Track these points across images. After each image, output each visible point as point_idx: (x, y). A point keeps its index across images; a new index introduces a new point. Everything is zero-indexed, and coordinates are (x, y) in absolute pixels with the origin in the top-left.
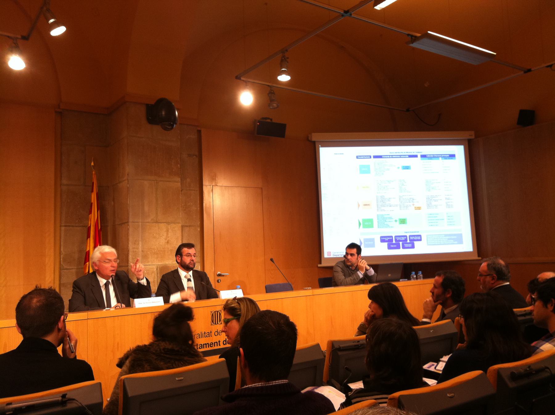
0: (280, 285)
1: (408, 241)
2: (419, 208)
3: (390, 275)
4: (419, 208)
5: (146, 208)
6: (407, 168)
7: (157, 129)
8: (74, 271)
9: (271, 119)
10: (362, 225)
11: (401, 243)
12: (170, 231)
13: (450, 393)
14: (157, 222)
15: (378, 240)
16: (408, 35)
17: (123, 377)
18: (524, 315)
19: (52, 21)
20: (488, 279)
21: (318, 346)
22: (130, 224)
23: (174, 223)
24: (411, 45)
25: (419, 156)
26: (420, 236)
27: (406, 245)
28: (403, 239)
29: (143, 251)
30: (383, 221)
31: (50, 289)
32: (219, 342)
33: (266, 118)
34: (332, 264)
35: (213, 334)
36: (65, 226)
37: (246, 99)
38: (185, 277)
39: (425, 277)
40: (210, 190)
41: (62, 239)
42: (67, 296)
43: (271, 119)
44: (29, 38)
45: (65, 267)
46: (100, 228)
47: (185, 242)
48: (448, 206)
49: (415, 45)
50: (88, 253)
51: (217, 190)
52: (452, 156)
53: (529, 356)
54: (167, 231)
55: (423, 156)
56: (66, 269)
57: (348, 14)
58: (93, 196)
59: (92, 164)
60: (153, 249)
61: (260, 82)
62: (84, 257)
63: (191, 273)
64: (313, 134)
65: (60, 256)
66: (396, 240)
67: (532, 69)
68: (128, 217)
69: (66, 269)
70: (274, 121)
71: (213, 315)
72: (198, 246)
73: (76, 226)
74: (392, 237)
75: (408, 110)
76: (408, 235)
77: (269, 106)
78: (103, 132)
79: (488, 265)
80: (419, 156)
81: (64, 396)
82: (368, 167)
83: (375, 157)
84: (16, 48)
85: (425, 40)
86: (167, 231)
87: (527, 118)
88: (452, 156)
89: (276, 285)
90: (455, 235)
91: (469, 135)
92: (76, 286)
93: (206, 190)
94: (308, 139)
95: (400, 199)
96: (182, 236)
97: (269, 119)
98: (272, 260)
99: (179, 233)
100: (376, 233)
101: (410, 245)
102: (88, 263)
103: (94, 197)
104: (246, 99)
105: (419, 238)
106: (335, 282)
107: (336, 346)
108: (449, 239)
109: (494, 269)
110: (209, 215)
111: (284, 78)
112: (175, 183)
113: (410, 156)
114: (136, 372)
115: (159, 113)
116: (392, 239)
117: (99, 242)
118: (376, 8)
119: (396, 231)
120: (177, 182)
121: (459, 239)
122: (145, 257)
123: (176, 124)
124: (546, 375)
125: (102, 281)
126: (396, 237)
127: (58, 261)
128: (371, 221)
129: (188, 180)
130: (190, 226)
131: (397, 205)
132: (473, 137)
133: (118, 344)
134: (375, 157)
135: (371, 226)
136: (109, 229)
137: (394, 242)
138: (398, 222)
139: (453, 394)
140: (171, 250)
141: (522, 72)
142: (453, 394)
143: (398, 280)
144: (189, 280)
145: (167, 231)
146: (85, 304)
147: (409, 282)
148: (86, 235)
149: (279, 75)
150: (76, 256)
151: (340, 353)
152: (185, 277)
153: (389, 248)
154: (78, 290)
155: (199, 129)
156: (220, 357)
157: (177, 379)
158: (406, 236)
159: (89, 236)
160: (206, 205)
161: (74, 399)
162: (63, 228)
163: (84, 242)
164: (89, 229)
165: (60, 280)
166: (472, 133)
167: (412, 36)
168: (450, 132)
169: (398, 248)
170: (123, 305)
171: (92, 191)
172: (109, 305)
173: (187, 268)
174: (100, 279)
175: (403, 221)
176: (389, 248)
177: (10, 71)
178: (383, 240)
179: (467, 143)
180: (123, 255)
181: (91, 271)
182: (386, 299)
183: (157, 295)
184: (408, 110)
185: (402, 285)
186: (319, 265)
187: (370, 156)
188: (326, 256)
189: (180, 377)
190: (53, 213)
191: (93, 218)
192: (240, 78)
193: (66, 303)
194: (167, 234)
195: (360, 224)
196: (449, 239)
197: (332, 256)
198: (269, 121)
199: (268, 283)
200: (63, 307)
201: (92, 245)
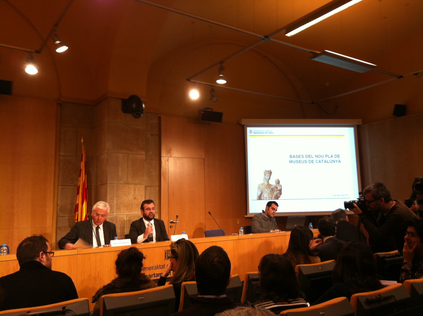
0: (216, 231)
3: (295, 225)
5: (120, 174)
8: (67, 218)
9: (212, 109)
12: (137, 190)
13: (322, 312)
14: (128, 184)
18: (389, 257)
19: (58, 42)
22: (108, 185)
33: (208, 108)
36: (62, 185)
37: (194, 95)
44: (41, 53)
45: (61, 215)
47: (147, 199)
49: (316, 59)
50: (77, 206)
51: (171, 160)
56: (62, 216)
59: (82, 141)
64: (243, 120)
68: (107, 181)
69: (62, 216)
72: (157, 202)
73: (69, 186)
75: (313, 103)
77: (211, 99)
78: (94, 119)
81: (64, 308)
84: (31, 59)
85: (323, 56)
86: (135, 190)
87: (400, 111)
89: (213, 231)
91: (359, 122)
93: (163, 160)
95: (306, 168)
96: (145, 194)
98: (209, 213)
99: (143, 193)
102: (77, 213)
103: (83, 165)
107: (251, 278)
110: (165, 178)
111: (221, 82)
112: (141, 155)
114: (113, 293)
115: (131, 106)
118: (286, 35)
123: (143, 113)
124: (392, 301)
129: (151, 153)
130: (151, 186)
132: (360, 124)
133: (98, 273)
139: (324, 313)
140: (137, 205)
141: (396, 78)
142: (324, 313)
145: (135, 190)
148: (76, 192)
150: (69, 207)
151: (253, 283)
155: (160, 116)
156: (169, 284)
157: (139, 298)
159: (78, 193)
161: (70, 310)
162: (60, 187)
163: (75, 198)
164: (79, 188)
165: (57, 225)
166: (360, 120)
171: (82, 161)
173: (149, 219)
177: (23, 70)
179: (356, 128)
183: (126, 237)
184: (313, 103)
186: (246, 216)
192: (190, 80)
194: (135, 192)
198: (210, 110)
201: (80, 200)
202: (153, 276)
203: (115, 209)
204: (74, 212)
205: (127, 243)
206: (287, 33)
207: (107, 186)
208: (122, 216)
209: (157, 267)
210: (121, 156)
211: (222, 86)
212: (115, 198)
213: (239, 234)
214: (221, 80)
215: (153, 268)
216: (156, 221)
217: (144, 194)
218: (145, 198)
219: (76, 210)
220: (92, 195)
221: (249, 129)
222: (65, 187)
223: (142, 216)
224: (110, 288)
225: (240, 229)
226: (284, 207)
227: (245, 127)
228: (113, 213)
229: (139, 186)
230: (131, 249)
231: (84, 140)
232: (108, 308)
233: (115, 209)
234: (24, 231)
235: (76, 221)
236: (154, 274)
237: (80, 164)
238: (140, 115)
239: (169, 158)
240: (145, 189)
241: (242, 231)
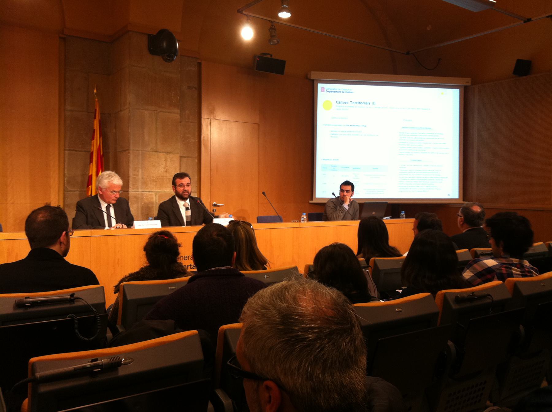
0: (271, 217)
3: (374, 213)
5: (146, 137)
7: (158, 59)
8: (77, 193)
9: (271, 55)
12: (169, 160)
13: (397, 308)
14: (156, 151)
17: (123, 284)
21: (296, 268)
22: (131, 152)
23: (173, 153)
31: (58, 208)
33: (266, 54)
34: (325, 201)
36: (69, 150)
37: (247, 33)
38: (184, 205)
39: (406, 217)
40: (209, 123)
42: (71, 214)
43: (271, 55)
45: (69, 189)
46: (102, 153)
47: (182, 171)
50: (90, 177)
51: (215, 124)
56: (70, 191)
58: (95, 122)
59: (95, 91)
60: (152, 176)
61: (266, 18)
62: (87, 180)
63: (188, 201)
64: (312, 72)
67: (532, 19)
68: (129, 145)
69: (70, 191)
70: (274, 57)
75: (408, 53)
77: (270, 41)
81: (72, 295)
86: (166, 160)
87: (523, 68)
89: (267, 217)
91: (467, 81)
92: (79, 207)
93: (204, 123)
94: (307, 78)
95: (393, 142)
97: (269, 54)
98: (263, 193)
99: (177, 164)
102: (90, 186)
104: (247, 33)
106: (326, 216)
110: (206, 147)
111: (285, 15)
112: (175, 115)
115: (161, 44)
117: (103, 166)
120: (177, 114)
122: (145, 183)
123: (177, 56)
124: (489, 301)
125: (104, 206)
127: (62, 185)
129: (187, 112)
130: (188, 157)
132: (469, 84)
133: (118, 259)
136: (111, 155)
140: (169, 179)
144: (187, 209)
145: (166, 160)
146: (87, 223)
147: (398, 220)
148: (88, 160)
149: (280, 12)
150: (79, 179)
152: (184, 205)
154: (81, 210)
157: (170, 288)
159: (91, 161)
160: (204, 137)
164: (92, 153)
165: (64, 202)
166: (469, 80)
168: (446, 78)
170: (125, 226)
171: (95, 118)
172: (110, 225)
173: (183, 199)
174: (102, 202)
179: (463, 89)
180: (125, 187)
181: (93, 194)
182: (373, 234)
183: (156, 219)
184: (408, 53)
186: (311, 202)
190: (57, 137)
193: (70, 221)
194: (166, 163)
198: (269, 56)
199: (261, 215)
200: (67, 224)
202: (189, 267)
203: (140, 184)
205: (157, 225)
207: (129, 152)
208: (150, 193)
210: (147, 113)
211: (285, 23)
212: (140, 170)
213: (300, 221)
214: (285, 12)
216: (192, 199)
217: (179, 167)
218: (180, 169)
219: (90, 183)
221: (320, 86)
222: (75, 152)
223: (174, 194)
224: (133, 277)
225: (302, 215)
226: (361, 193)
227: (315, 82)
229: (172, 155)
230: (162, 233)
231: (97, 90)
234: (22, 203)
237: (93, 124)
238: (172, 57)
239: (212, 121)
240: (180, 160)
241: (305, 217)
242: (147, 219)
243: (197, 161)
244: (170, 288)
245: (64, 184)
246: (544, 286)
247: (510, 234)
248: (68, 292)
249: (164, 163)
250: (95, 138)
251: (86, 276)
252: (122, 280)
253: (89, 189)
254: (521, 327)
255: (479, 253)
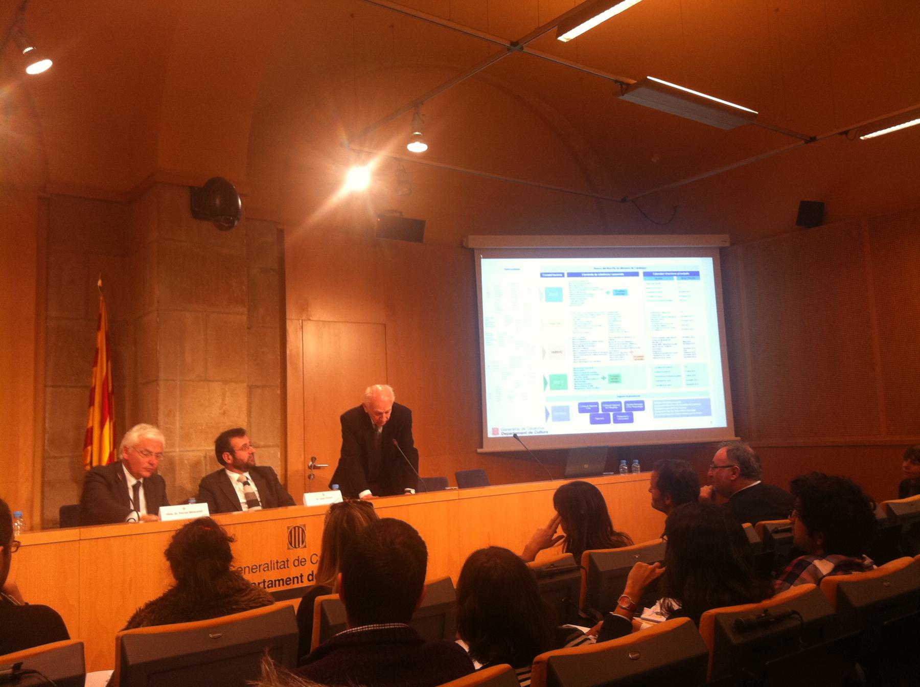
1: (624, 411)
2: (641, 358)
3: (586, 466)
4: (641, 358)
5: (188, 358)
6: (622, 293)
8: (67, 460)
10: (548, 386)
11: (611, 414)
12: (228, 394)
14: (206, 380)
15: (574, 409)
16: (616, 81)
20: (726, 472)
22: (161, 383)
24: (621, 98)
25: (641, 274)
26: (643, 402)
27: (620, 417)
28: (615, 407)
29: (181, 428)
30: (583, 378)
32: (301, 576)
35: (291, 563)
36: (52, 386)
41: (48, 407)
45: (52, 454)
48: (688, 355)
49: (627, 97)
50: (90, 432)
52: (695, 274)
53: (770, 596)
54: (224, 395)
55: (648, 274)
56: (55, 457)
57: (518, 47)
58: (99, 337)
59: (100, 283)
64: (470, 237)
65: (44, 436)
66: (603, 409)
69: (55, 457)
71: (291, 532)
74: (597, 403)
75: (624, 201)
76: (623, 400)
79: (728, 451)
80: (641, 274)
81: (17, 667)
82: (559, 290)
83: (571, 275)
85: (643, 90)
86: (224, 395)
88: (695, 274)
90: (696, 401)
93: (291, 327)
95: (609, 345)
100: (572, 397)
101: (626, 418)
103: (101, 340)
105: (641, 406)
108: (689, 408)
109: (738, 458)
112: (239, 316)
113: (627, 274)
116: (598, 408)
118: (560, 38)
119: (603, 394)
121: (705, 408)
123: (238, 220)
126: (603, 403)
128: (564, 378)
130: (264, 387)
131: (605, 353)
132: (727, 244)
134: (571, 275)
135: (564, 387)
137: (600, 412)
138: (607, 380)
143: (599, 474)
145: (224, 395)
148: (87, 401)
153: (593, 421)
155: (281, 227)
157: (211, 636)
158: (620, 403)
159: (92, 403)
160: (291, 351)
161: (34, 672)
163: (84, 414)
164: (93, 390)
167: (622, 83)
169: (607, 421)
171: (99, 328)
175: (615, 379)
176: (593, 421)
178: (582, 410)
179: (718, 257)
184: (624, 201)
185: (603, 483)
187: (563, 274)
188: (490, 435)
189: (215, 633)
191: (98, 376)
194: (223, 400)
195: (545, 383)
196: (689, 408)
197: (500, 435)
203: (177, 439)
204: (83, 445)
205: (200, 510)
206: (561, 35)
207: (158, 385)
209: (268, 567)
212: (178, 414)
215: (262, 567)
219: (89, 440)
220: (124, 408)
228: (173, 446)
232: (132, 660)
233: (177, 439)
235: (88, 468)
236: (264, 582)
238: (232, 223)
242: (186, 502)
243: (279, 392)
244: (211, 636)
245: (44, 446)
246: (889, 586)
247: (839, 517)
248: (11, 660)
249: (220, 400)
250: (99, 364)
251: (46, 624)
252: (135, 622)
253: (87, 452)
254: (858, 668)
255: (770, 529)
